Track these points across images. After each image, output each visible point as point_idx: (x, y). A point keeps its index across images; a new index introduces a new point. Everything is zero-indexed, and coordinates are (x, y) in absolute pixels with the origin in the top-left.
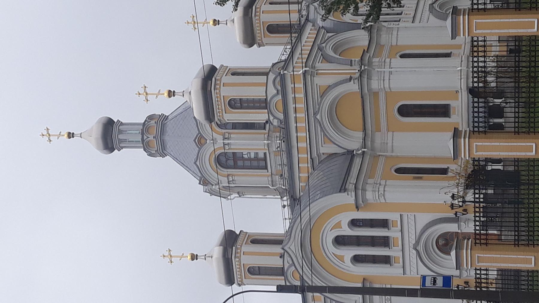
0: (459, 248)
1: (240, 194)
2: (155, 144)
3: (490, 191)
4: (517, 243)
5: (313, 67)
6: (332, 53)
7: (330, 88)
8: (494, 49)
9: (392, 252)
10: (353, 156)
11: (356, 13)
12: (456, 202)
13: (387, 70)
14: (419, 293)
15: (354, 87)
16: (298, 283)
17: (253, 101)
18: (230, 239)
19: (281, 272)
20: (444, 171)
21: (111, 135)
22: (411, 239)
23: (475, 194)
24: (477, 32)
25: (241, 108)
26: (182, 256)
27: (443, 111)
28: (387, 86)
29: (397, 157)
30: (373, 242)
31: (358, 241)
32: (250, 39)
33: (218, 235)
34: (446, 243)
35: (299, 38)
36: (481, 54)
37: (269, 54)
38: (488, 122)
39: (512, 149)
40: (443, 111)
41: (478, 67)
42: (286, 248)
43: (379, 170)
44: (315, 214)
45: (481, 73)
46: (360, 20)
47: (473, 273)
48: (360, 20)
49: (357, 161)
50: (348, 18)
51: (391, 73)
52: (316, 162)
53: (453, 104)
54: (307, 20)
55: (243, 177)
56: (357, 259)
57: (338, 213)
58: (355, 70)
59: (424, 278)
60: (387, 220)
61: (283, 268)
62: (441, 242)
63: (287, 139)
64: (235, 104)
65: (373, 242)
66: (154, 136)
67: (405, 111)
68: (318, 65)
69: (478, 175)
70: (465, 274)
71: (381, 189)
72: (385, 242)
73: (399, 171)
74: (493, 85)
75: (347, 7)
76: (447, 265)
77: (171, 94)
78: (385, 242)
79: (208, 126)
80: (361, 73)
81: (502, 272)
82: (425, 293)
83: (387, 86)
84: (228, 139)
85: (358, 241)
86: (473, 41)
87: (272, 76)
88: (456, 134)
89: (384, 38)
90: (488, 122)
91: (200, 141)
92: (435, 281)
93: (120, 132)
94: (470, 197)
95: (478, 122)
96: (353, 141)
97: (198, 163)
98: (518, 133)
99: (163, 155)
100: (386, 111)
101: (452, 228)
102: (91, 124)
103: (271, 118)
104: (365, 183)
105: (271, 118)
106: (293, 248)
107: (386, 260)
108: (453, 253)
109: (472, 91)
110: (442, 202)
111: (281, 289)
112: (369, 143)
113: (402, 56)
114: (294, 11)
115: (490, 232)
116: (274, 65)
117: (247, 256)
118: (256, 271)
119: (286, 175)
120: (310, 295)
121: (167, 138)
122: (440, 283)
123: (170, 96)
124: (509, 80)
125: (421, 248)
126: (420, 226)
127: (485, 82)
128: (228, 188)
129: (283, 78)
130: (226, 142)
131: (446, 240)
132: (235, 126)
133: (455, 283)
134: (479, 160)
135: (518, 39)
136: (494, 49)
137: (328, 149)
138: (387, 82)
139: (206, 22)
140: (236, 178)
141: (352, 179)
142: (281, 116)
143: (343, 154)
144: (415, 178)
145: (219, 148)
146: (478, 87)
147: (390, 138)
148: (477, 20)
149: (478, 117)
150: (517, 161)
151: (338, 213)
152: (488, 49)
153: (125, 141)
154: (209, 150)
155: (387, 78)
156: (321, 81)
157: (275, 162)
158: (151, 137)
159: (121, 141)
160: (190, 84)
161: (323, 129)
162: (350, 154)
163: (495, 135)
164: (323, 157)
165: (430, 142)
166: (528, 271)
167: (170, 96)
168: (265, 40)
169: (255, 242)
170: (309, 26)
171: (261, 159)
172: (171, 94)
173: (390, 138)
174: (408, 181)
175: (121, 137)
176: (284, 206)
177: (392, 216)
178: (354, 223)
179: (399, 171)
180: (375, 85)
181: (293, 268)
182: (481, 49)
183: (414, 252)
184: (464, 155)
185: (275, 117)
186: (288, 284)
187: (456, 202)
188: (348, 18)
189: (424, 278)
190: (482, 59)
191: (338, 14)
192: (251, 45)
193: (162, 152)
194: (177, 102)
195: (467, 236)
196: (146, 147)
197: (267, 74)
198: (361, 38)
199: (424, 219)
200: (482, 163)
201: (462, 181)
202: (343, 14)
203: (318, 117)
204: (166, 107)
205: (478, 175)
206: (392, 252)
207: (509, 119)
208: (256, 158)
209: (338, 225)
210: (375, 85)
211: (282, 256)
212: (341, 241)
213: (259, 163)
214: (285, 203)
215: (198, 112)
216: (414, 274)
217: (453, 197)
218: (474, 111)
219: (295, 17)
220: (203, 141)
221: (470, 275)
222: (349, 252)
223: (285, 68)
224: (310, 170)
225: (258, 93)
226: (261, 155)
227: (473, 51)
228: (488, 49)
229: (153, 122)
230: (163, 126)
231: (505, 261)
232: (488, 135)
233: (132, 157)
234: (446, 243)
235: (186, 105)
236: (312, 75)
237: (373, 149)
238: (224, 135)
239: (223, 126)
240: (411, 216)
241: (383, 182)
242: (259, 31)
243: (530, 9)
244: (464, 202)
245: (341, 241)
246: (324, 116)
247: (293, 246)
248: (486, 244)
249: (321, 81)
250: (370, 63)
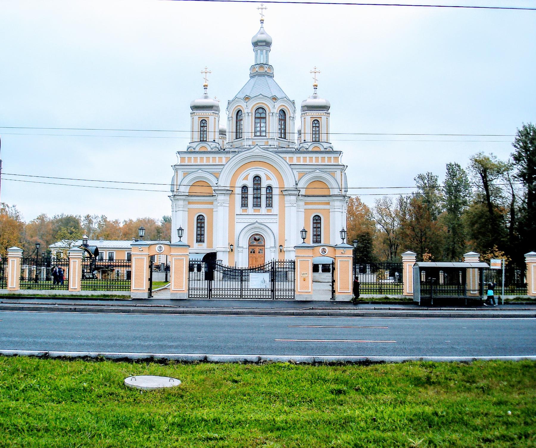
9: (250, 209)
22: (260, 219)
30: (257, 198)
51: (342, 212)
56: (245, 188)
62: (257, 237)
65: (257, 198)
66: (262, 71)
72: (257, 205)
78: (257, 205)
97: (261, 96)
107: (244, 205)
110: (286, 239)
115: (27, 277)
131: (259, 240)
158: (266, 69)
159: (257, 51)
177: (275, 209)
178: (269, 188)
183: (255, 221)
206: (250, 209)
209: (268, 178)
212: (257, 179)
222: (250, 184)
233: (250, 57)
245: (257, 179)
246: (318, 173)
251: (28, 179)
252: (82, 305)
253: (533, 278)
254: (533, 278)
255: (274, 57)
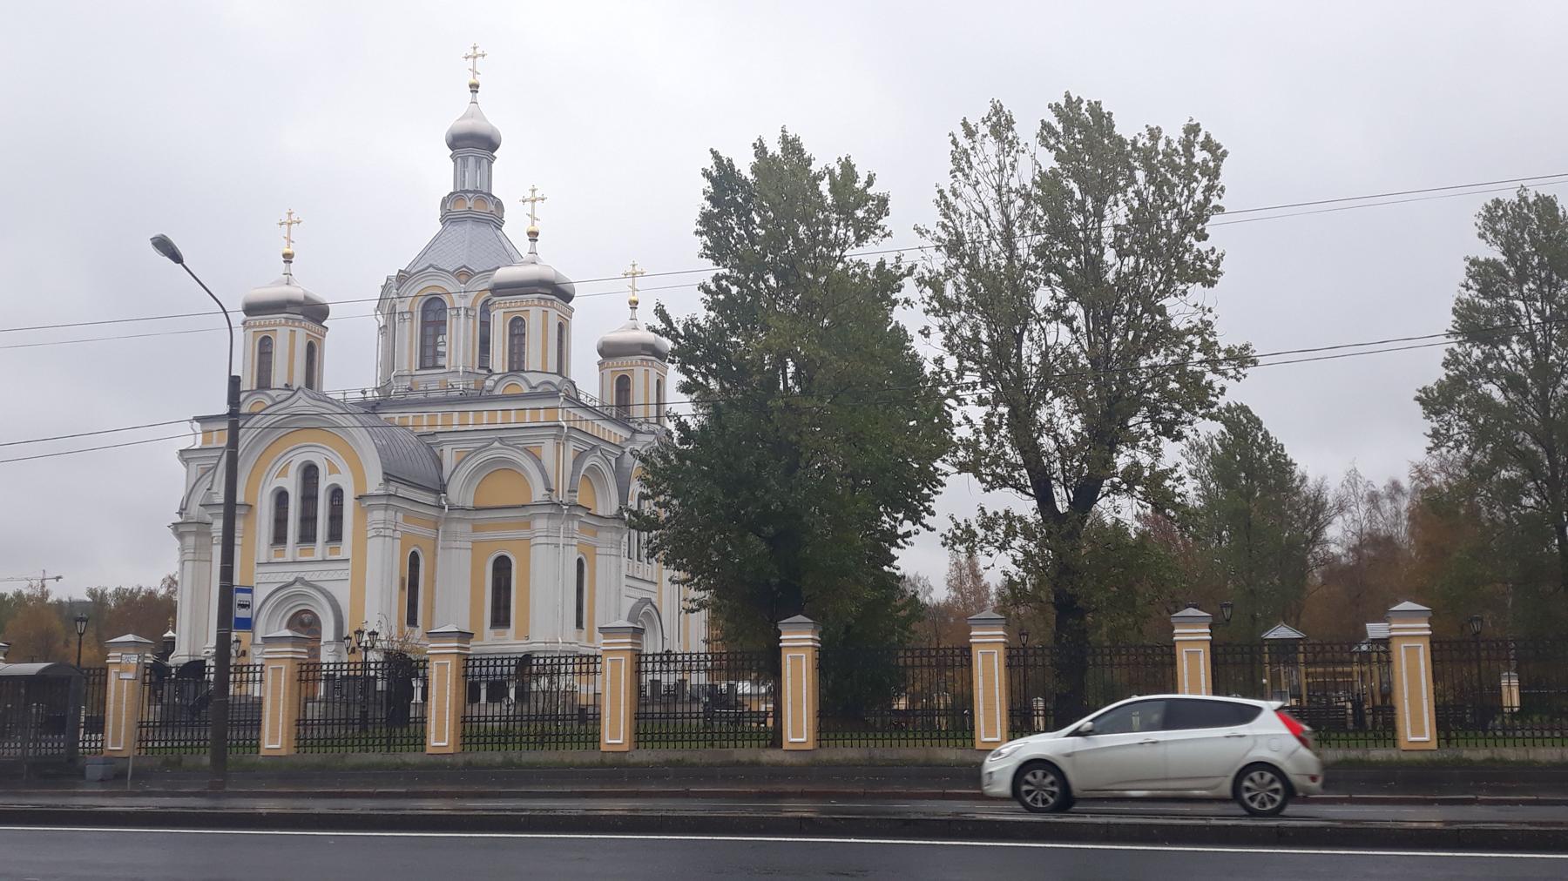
0: (294, 641)
1: (383, 329)
2: (459, 209)
3: (380, 685)
4: (301, 723)
5: (568, 438)
6: (587, 463)
7: (537, 460)
8: (584, 686)
10: (437, 492)
11: (643, 497)
12: (366, 637)
13: (561, 541)
14: (227, 583)
15: (539, 494)
16: (244, 409)
17: (521, 353)
18: (315, 312)
19: (264, 383)
20: (412, 620)
21: (474, 146)
22: (311, 573)
23: (376, 663)
24: (607, 663)
25: (512, 335)
26: (290, 241)
27: (501, 617)
28: (539, 540)
29: (435, 555)
30: (308, 520)
31: (309, 498)
32: (610, 351)
33: (320, 294)
34: (305, 624)
35: (608, 419)
36: (1238, 657)
37: (588, 377)
38: (478, 680)
39: (441, 713)
40: (501, 617)
41: (559, 664)
42: (300, 393)
43: (417, 530)
44: (349, 434)
45: (553, 666)
46: (633, 504)
47: (258, 662)
48: (633, 504)
49: (430, 499)
50: (636, 488)
51: (557, 546)
52: (430, 440)
53: (511, 632)
54: (634, 431)
55: (409, 335)
56: (281, 497)
57: (352, 468)
58: (562, 496)
59: (250, 591)
60: (340, 539)
61: (269, 388)
63: (465, 398)
64: (517, 328)
65: (308, 520)
66: (472, 208)
67: (502, 567)
68: (571, 445)
69: (404, 669)
70: (256, 651)
71: (388, 532)
72: (308, 536)
73: (414, 558)
74: (534, 686)
75: (649, 485)
76: (270, 624)
77: (533, 236)
78: (308, 536)
79: (486, 286)
80: (558, 505)
81: (258, 704)
82: (227, 592)
83: (539, 540)
84: (467, 315)
85: (309, 498)
86: (596, 657)
87: (556, 380)
88: (465, 636)
89: (606, 536)
90: (478, 680)
91: (464, 274)
92: (243, 606)
93: (478, 161)
94: (373, 656)
95: (502, 666)
96: (458, 492)
98: (464, 722)
99: (443, 220)
100: (501, 540)
101: (328, 633)
102: (494, 116)
103: (496, 378)
104: (397, 509)
105: (496, 378)
106: (301, 402)
107: (280, 538)
108: (288, 633)
109: (527, 659)
111: (234, 382)
112: (456, 515)
113: (580, 562)
114: (647, 411)
116: (573, 383)
117: (288, 339)
118: (265, 348)
119: (411, 397)
120: (225, 425)
121: (468, 226)
122: (241, 613)
123: (529, 234)
124: (540, 705)
125: (298, 588)
126: (328, 586)
127: (538, 674)
128: (393, 312)
129: (554, 395)
130: (462, 312)
132: (485, 325)
133: (244, 636)
134: (425, 668)
135: (597, 718)
136: (584, 686)
137: (449, 457)
138: (544, 540)
139: (634, 290)
140: (407, 324)
141: (403, 491)
142: (498, 392)
143: (441, 479)
144: (403, 580)
145: (452, 301)
146: (531, 665)
147: (463, 545)
148: (625, 663)
149: (495, 666)
150: (423, 720)
151: (352, 468)
152: (584, 678)
153: (465, 165)
154: (451, 285)
155: (550, 540)
156: (548, 450)
157: (431, 381)
158: (469, 204)
159: (465, 160)
160: (552, 261)
161: (478, 450)
162: (441, 488)
163: (461, 690)
164: (437, 450)
165: (456, 599)
166: (258, 739)
167: (529, 234)
168: (607, 372)
169: (311, 349)
170: (626, 434)
171: (435, 361)
172: (533, 236)
173: (463, 545)
174: (399, 569)
175: (471, 161)
176: (364, 392)
178: (337, 493)
179: (414, 558)
180: (541, 524)
181: (269, 403)
182: (584, 667)
184: (432, 647)
185: (496, 383)
186: (242, 397)
187: (366, 637)
188: (636, 488)
189: (250, 591)
190: (570, 669)
191: (640, 472)
192: (601, 352)
193: (448, 218)
194: (523, 245)
195: (315, 652)
196: (455, 197)
197: (560, 373)
198: (608, 504)
199: (343, 593)
200: (421, 673)
201: (396, 646)
202: (640, 479)
203: (496, 444)
204: (514, 228)
205: (404, 669)
207: (485, 706)
208: (437, 354)
209: (333, 469)
210: (541, 524)
211: (288, 387)
212: (310, 473)
213: (429, 356)
214: (369, 394)
215: (505, 274)
216: (257, 578)
217: (373, 633)
218: (501, 659)
219: (638, 412)
220: (463, 278)
221: (256, 656)
222: (292, 484)
223: (568, 398)
224: (419, 430)
225: (533, 359)
226: (441, 361)
227: (581, 657)
228: (584, 678)
229: (493, 207)
230: (488, 222)
231: (275, 706)
232: (462, 680)
234: (305, 624)
235: (517, 257)
236: (556, 437)
237: (448, 520)
238: (473, 308)
239: (486, 308)
240: (347, 575)
241: (398, 535)
242: (621, 364)
243: (638, 733)
244: (366, 649)
245: (310, 473)
246: (497, 451)
247: (302, 403)
248: (300, 680)
249: (548, 450)
250: (572, 517)
251: (1430, 341)
252: (1163, 815)
253: (1425, 702)
254: (1425, 702)
255: (507, 178)
